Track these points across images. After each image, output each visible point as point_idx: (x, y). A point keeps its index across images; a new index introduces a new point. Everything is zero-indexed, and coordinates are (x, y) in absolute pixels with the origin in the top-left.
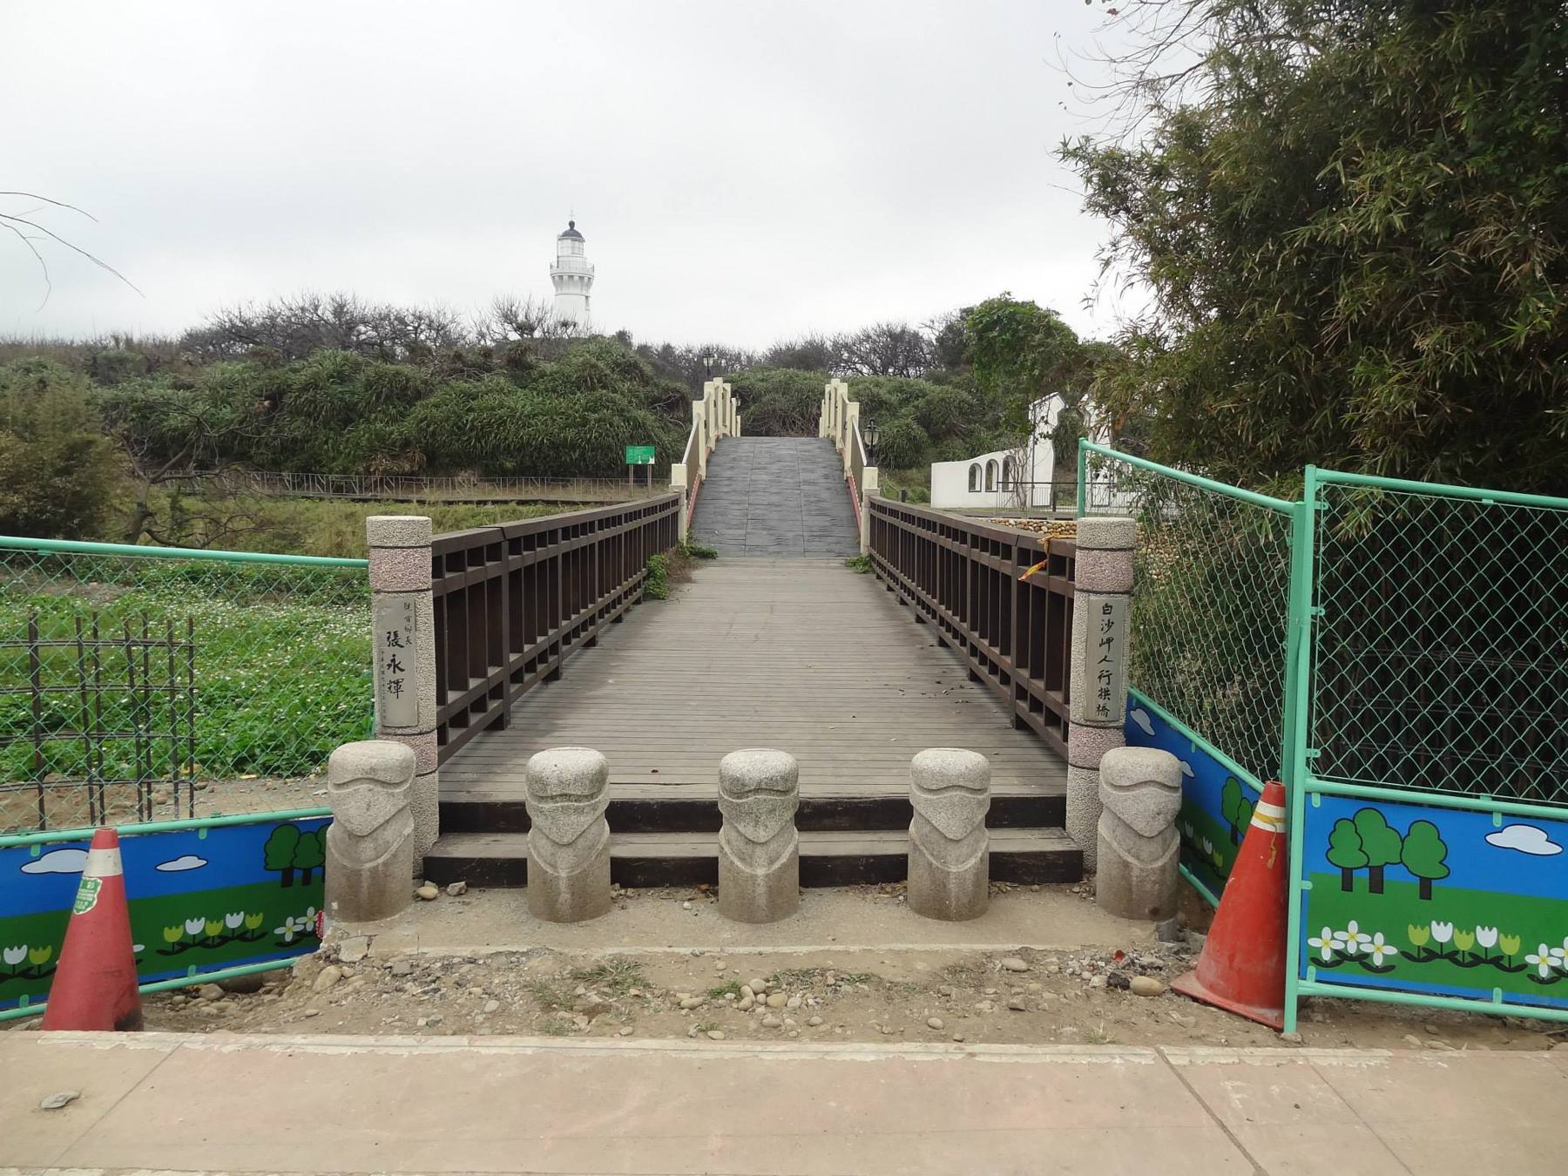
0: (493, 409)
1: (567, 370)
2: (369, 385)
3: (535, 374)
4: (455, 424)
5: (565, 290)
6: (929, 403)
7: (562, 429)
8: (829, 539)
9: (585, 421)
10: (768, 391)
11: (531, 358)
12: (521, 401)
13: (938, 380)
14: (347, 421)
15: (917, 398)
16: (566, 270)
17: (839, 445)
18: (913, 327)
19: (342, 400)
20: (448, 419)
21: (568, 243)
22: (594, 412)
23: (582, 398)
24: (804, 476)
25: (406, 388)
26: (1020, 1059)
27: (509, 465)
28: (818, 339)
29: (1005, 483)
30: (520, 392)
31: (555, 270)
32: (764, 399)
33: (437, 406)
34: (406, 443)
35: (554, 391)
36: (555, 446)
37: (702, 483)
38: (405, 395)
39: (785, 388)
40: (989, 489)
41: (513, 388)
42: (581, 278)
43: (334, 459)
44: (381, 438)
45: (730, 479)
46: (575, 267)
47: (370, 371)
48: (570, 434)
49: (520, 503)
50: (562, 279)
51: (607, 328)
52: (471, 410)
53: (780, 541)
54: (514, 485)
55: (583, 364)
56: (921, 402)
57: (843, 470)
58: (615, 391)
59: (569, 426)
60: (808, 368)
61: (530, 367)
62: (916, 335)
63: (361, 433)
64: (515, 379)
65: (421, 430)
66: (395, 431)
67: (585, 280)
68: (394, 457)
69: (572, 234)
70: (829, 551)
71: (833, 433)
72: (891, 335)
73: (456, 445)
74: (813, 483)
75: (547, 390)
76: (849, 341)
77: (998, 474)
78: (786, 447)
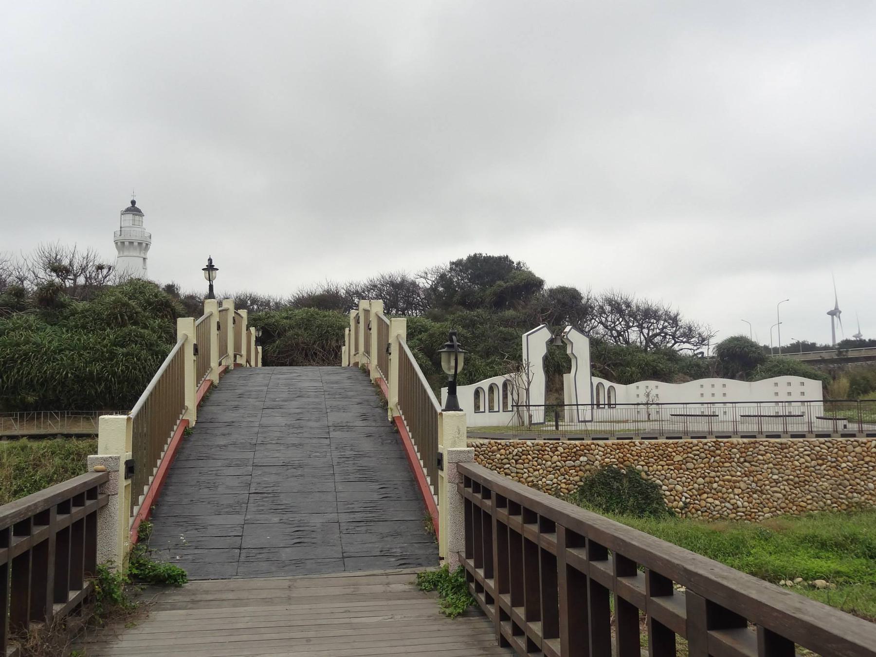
0: (18, 345)
1: (99, 308)
3: (66, 312)
5: (125, 254)
6: (431, 336)
7: (87, 363)
8: (383, 528)
9: (113, 355)
10: (291, 327)
11: (65, 298)
12: (49, 337)
13: (436, 319)
15: (420, 332)
17: (375, 374)
18: (411, 276)
21: (130, 217)
22: (122, 346)
23: (111, 334)
24: (334, 418)
26: (382, 571)
27: (30, 399)
28: (333, 289)
29: (505, 404)
30: (49, 329)
31: (118, 238)
32: (290, 333)
35: (84, 327)
36: (78, 379)
37: (187, 434)
39: (307, 324)
40: (491, 409)
41: (42, 324)
42: (140, 244)
45: (230, 424)
46: (135, 234)
48: (96, 368)
49: (32, 437)
50: (122, 245)
51: (162, 280)
53: (301, 537)
54: (32, 419)
55: (114, 302)
56: (424, 336)
57: (384, 405)
58: (145, 327)
59: (96, 360)
60: (327, 308)
61: (63, 305)
62: (414, 284)
67: (143, 246)
69: (133, 209)
70: (385, 554)
71: (362, 360)
72: (392, 284)
75: (76, 326)
76: (359, 289)
77: (498, 395)
78: (308, 377)
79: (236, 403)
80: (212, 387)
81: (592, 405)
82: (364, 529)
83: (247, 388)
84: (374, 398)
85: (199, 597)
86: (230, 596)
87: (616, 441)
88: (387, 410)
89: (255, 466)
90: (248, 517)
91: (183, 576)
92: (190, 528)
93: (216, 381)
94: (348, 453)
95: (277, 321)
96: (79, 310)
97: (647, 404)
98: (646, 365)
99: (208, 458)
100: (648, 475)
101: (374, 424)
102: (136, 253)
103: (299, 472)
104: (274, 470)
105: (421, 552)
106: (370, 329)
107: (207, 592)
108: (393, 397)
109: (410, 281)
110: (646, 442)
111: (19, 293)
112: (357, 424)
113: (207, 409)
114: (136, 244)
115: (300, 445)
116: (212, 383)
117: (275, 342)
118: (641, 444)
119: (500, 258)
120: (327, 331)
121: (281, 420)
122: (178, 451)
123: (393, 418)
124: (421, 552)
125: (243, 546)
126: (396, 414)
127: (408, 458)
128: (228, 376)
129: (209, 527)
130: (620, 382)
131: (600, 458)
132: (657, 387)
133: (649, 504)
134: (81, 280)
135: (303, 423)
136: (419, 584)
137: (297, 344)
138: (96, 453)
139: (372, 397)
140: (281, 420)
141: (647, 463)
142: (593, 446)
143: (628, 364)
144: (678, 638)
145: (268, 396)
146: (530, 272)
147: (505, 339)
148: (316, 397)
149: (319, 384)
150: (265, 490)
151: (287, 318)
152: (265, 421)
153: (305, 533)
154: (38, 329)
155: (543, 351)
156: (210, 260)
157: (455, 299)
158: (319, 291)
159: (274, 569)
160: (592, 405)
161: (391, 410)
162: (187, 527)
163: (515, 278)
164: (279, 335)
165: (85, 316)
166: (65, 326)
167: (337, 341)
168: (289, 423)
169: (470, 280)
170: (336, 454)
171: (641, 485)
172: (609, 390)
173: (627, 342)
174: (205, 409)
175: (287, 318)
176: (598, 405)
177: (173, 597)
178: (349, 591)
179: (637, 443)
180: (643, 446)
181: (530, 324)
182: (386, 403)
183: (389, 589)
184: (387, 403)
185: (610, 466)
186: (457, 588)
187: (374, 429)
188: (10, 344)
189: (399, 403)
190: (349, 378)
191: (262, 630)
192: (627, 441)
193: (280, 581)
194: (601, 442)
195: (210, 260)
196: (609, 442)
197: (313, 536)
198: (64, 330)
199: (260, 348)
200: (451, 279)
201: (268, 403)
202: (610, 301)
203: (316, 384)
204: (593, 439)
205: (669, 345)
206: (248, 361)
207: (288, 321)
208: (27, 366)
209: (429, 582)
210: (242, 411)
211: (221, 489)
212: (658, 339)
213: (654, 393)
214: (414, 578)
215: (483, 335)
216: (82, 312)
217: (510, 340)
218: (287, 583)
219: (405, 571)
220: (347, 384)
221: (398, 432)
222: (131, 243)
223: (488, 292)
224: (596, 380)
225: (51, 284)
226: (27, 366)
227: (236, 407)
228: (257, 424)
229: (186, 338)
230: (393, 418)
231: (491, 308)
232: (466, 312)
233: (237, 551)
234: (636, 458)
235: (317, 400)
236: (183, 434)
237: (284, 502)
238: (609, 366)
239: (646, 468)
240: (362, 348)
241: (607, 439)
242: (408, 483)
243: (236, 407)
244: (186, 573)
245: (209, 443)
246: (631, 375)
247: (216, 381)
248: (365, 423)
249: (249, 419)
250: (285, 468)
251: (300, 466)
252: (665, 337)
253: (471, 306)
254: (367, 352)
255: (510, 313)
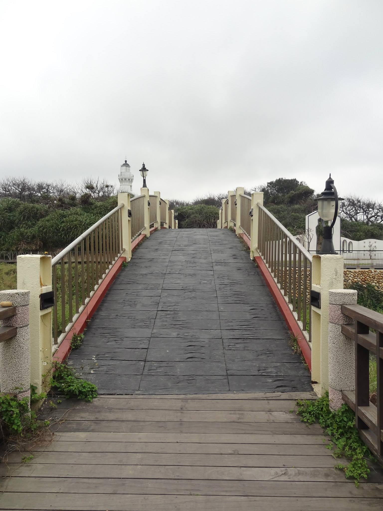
0: (72, 221)
2: (21, 213)
3: (93, 207)
4: (56, 228)
5: (123, 184)
10: (193, 213)
11: (91, 200)
14: (12, 228)
16: (123, 177)
17: (239, 231)
19: (9, 219)
20: (52, 226)
21: (124, 167)
24: (215, 257)
25: (37, 213)
28: (212, 197)
30: (86, 214)
32: (192, 216)
33: (48, 221)
34: (34, 237)
37: (124, 266)
38: (35, 216)
39: (200, 212)
41: (82, 212)
43: (4, 244)
44: (22, 234)
45: (151, 260)
46: (127, 176)
47: (22, 207)
50: (122, 180)
52: (63, 222)
57: (248, 249)
61: (92, 204)
63: (15, 233)
64: (85, 210)
65: (39, 231)
66: (30, 232)
68: (28, 243)
69: (126, 164)
73: (56, 237)
74: (225, 264)
75: (97, 213)
78: (199, 234)
79: (157, 247)
80: (145, 238)
81: (340, 251)
82: (241, 346)
83: (165, 239)
84: (240, 245)
85: (102, 416)
86: (129, 416)
87: (361, 270)
88: (249, 253)
89: (163, 289)
90: (155, 331)
91: (92, 391)
92: (112, 339)
93: (148, 235)
94: (226, 281)
95: (186, 211)
96: (98, 206)
97: (370, 251)
98: (368, 231)
99: (134, 283)
100: (379, 288)
101: (241, 261)
102: (128, 184)
103: (193, 295)
104: (175, 293)
105: (292, 373)
106: (236, 204)
107: (110, 410)
108: (254, 244)
109: (248, 192)
110: (378, 271)
111: (73, 198)
112: (230, 261)
113: (141, 250)
114: (127, 179)
115: (194, 275)
116: (145, 236)
117: (185, 220)
118: (375, 272)
119: (292, 180)
120: (210, 215)
121: (182, 258)
122: (115, 278)
123: (254, 257)
124: (292, 373)
125: (148, 359)
126: (256, 255)
127: (268, 285)
128: (156, 232)
129: (125, 339)
130: (354, 240)
131: (351, 279)
132: (375, 242)
133: (379, 303)
134: (101, 194)
135: (196, 260)
136: (300, 414)
137: (196, 221)
138: (13, 286)
139: (238, 244)
140: (182, 258)
141: (378, 282)
142: (348, 272)
143: (358, 231)
144: (371, 357)
145: (176, 243)
146: (307, 186)
147: (295, 219)
148: (205, 244)
149: (206, 237)
150: (168, 309)
151: (191, 209)
152: (173, 258)
153: (196, 347)
154: (81, 214)
155: (316, 224)
156: (144, 165)
157: (270, 200)
158: (206, 198)
159: (170, 385)
160: (340, 251)
161: (253, 252)
162: (109, 338)
163: (299, 189)
164: (188, 217)
165: (101, 209)
166: (92, 213)
167: (214, 220)
168: (187, 260)
169: (277, 191)
170: (218, 281)
171: (375, 293)
172: (349, 244)
173: (356, 220)
174: (139, 250)
175: (191, 209)
176: (343, 251)
177: (83, 414)
178: (234, 417)
179: (373, 271)
180: (376, 273)
181: (308, 211)
182: (248, 248)
183: (272, 418)
184: (249, 249)
185: (357, 283)
186: (345, 432)
187: (243, 265)
188: (69, 221)
189: (259, 247)
190: (223, 234)
191: (150, 484)
192: (367, 270)
193: (172, 401)
194: (352, 270)
195: (144, 165)
196: (357, 270)
197: (202, 351)
198: (92, 215)
199: (177, 221)
200: (268, 191)
201: (176, 248)
202: (349, 200)
203: (205, 237)
204: (347, 268)
205: (379, 222)
206: (170, 227)
207: (191, 211)
208: (76, 231)
209: (310, 413)
210: (159, 252)
211: (139, 307)
212: (373, 219)
213: (374, 245)
214: (292, 405)
215: (284, 217)
216: (100, 207)
217: (297, 219)
218: (179, 404)
219: (285, 396)
220: (222, 237)
221: (258, 267)
222: (125, 179)
223: (286, 197)
224: (343, 239)
225: (86, 194)
226: (76, 231)
227: (157, 250)
228: (167, 260)
229: (123, 206)
230: (254, 257)
231: (288, 204)
232: (275, 206)
233: (142, 363)
234: (372, 279)
235: (205, 246)
236: (121, 266)
237: (182, 319)
238: (348, 232)
239: (377, 284)
240: (229, 218)
241: (355, 269)
242: (271, 306)
243: (157, 250)
244: (96, 388)
245: (136, 273)
246: (360, 236)
247: (148, 235)
248: (235, 261)
249: (163, 257)
250: (183, 291)
251: (194, 290)
252: (376, 218)
253: (278, 204)
254: (234, 219)
255: (297, 206)
